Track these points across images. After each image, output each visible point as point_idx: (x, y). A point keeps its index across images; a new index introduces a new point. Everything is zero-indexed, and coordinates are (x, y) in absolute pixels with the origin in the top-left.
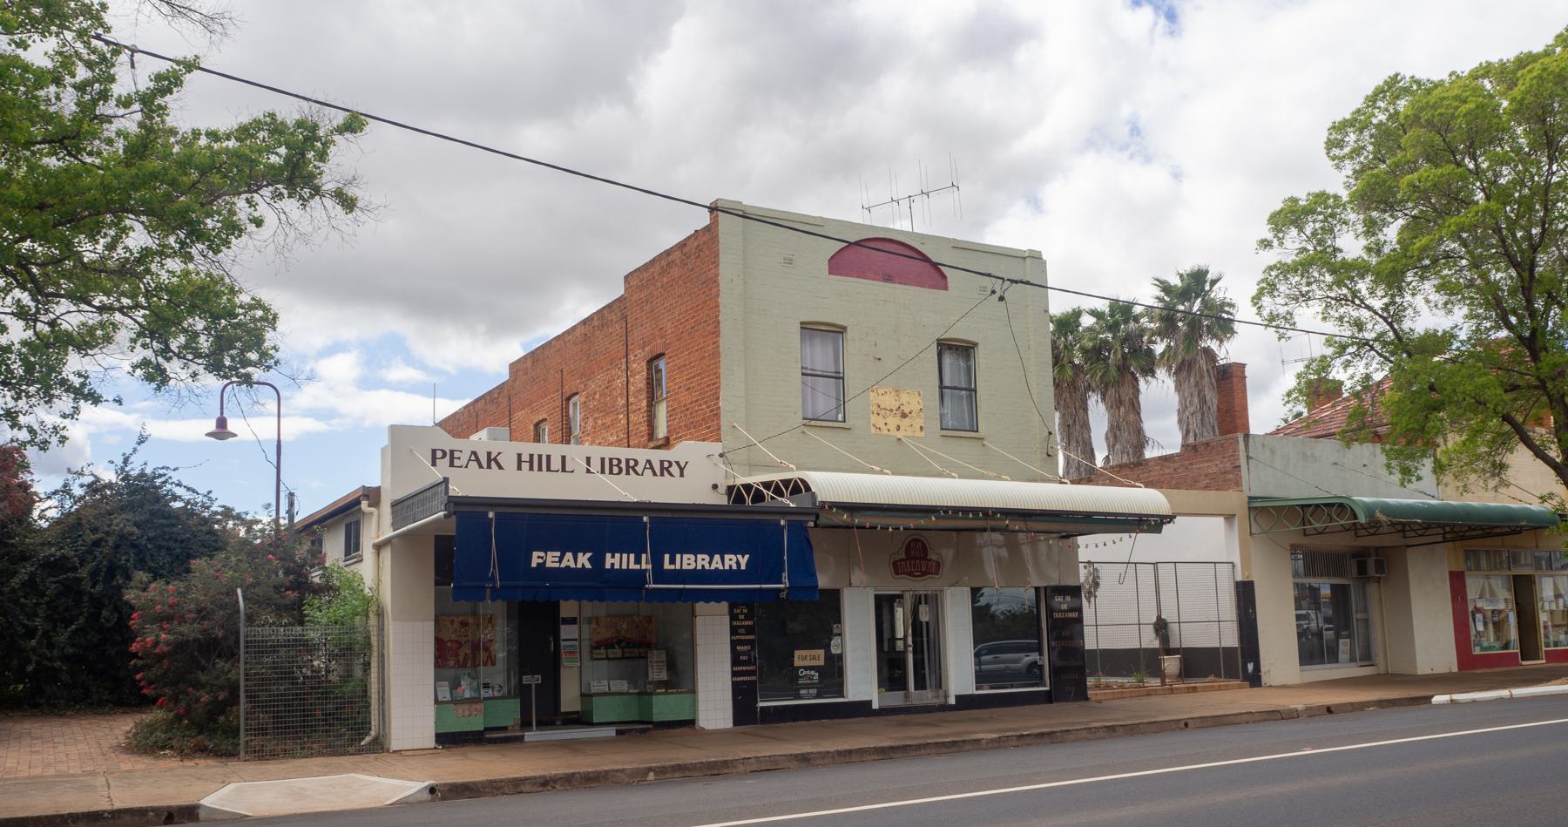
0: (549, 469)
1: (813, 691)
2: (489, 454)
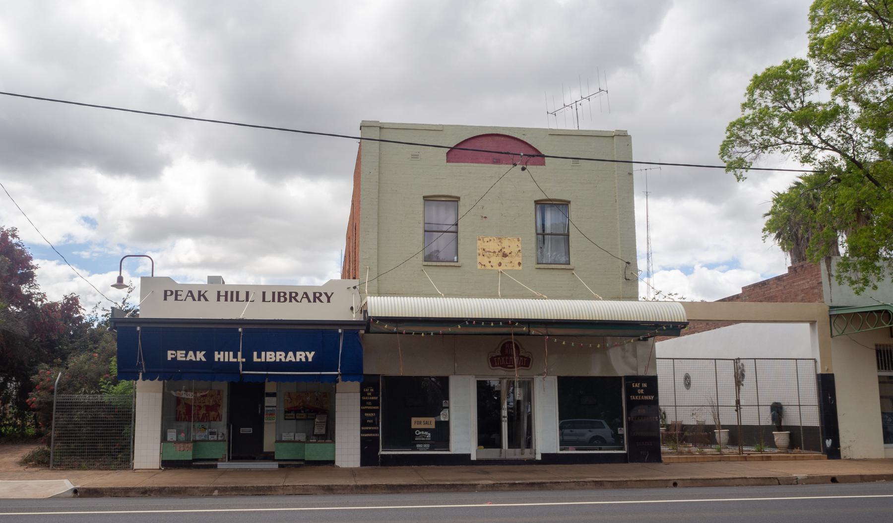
0: (237, 300)
1: (428, 446)
2: (200, 292)
